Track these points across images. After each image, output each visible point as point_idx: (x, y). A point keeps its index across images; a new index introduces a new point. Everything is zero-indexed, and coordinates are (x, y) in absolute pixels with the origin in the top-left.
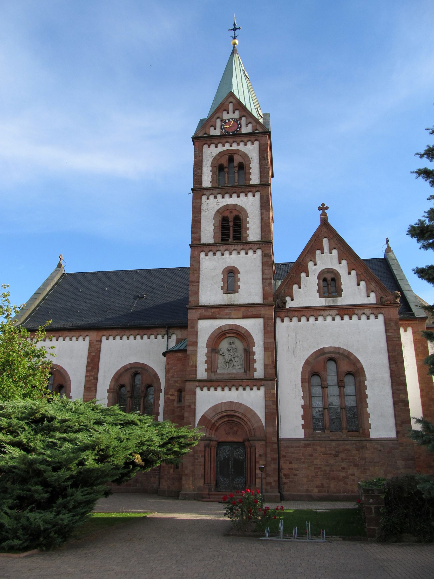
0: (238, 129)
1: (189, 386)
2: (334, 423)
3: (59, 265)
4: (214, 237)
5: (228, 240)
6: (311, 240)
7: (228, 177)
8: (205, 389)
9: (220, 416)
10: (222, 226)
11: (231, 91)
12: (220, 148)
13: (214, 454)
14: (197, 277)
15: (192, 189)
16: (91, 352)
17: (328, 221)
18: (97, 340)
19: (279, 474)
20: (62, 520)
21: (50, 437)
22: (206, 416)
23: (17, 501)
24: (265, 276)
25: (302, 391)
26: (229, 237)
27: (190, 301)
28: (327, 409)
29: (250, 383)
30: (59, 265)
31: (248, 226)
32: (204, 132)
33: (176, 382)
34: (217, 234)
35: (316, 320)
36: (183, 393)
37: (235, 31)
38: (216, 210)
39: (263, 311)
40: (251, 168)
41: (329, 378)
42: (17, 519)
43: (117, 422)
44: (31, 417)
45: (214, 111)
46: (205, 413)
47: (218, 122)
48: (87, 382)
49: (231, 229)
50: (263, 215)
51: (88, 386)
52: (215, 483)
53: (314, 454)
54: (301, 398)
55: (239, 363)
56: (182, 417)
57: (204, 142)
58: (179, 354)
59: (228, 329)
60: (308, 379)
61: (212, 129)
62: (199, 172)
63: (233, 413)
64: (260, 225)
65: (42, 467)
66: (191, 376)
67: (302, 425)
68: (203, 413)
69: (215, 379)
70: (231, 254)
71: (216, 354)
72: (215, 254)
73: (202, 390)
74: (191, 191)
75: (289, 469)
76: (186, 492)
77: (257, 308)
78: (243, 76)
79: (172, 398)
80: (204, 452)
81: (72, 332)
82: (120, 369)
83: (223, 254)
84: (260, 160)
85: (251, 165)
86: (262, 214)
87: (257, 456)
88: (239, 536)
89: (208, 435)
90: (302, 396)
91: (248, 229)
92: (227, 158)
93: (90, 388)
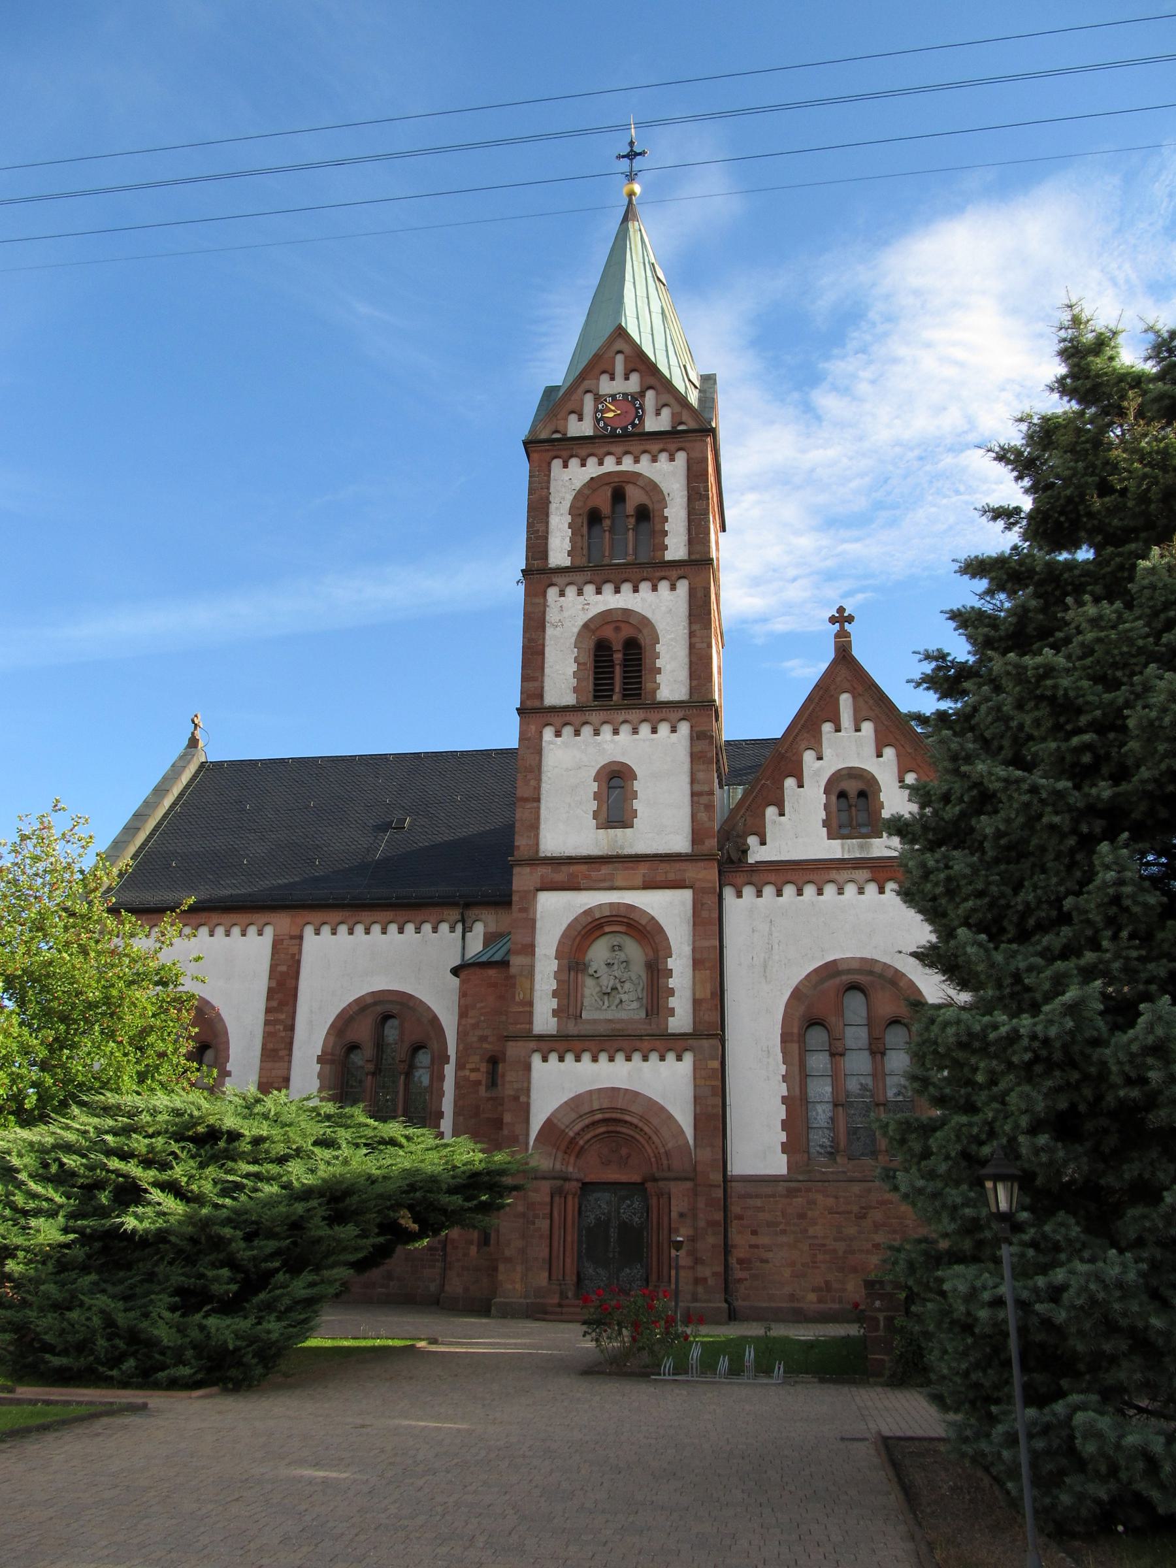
0: (637, 422)
1: (513, 1050)
2: (858, 1139)
3: (193, 742)
4: (575, 690)
5: (611, 696)
6: (810, 699)
7: (612, 540)
8: (553, 1057)
9: (587, 1122)
10: (596, 661)
11: (620, 324)
12: (593, 469)
13: (573, 1211)
14: (535, 788)
15: (522, 571)
16: (277, 965)
17: (853, 653)
18: (293, 933)
19: (726, 1260)
20: (269, 1332)
21: (228, 1172)
22: (555, 1121)
23: (177, 1299)
24: (697, 788)
25: (784, 1063)
26: (612, 690)
27: (518, 847)
28: (842, 1105)
29: (658, 1042)
30: (193, 742)
31: (659, 663)
32: (553, 428)
33: (483, 1039)
34: (584, 684)
35: (820, 892)
36: (500, 1066)
37: (631, 160)
38: (582, 624)
39: (692, 872)
40: (666, 519)
41: (850, 1032)
42: (181, 1330)
43: (359, 1141)
44: (188, 1131)
45: (577, 374)
46: (552, 1114)
47: (589, 403)
48: (268, 1036)
49: (618, 670)
50: (695, 636)
51: (270, 1046)
52: (574, 1278)
53: (809, 1212)
54: (780, 1078)
55: (633, 996)
56: (498, 1123)
57: (554, 453)
58: (492, 972)
59: (608, 914)
60: (799, 1034)
61: (573, 418)
62: (540, 527)
63: (618, 1116)
64: (686, 660)
65: (227, 1232)
66: (519, 1026)
67: (782, 1143)
68: (548, 1115)
69: (575, 1033)
70: (616, 732)
71: (580, 976)
72: (577, 733)
73: (545, 1059)
74: (520, 576)
75: (751, 1246)
76: (507, 1300)
77: (678, 865)
78: (650, 280)
79: (474, 1076)
80: (549, 1207)
81: (231, 915)
82: (350, 1005)
83: (597, 733)
84: (690, 499)
85: (666, 512)
86: (692, 634)
87: (674, 1215)
88: (610, 1374)
89: (558, 1166)
90: (783, 1076)
91: (659, 671)
92: (609, 494)
93: (275, 1051)
